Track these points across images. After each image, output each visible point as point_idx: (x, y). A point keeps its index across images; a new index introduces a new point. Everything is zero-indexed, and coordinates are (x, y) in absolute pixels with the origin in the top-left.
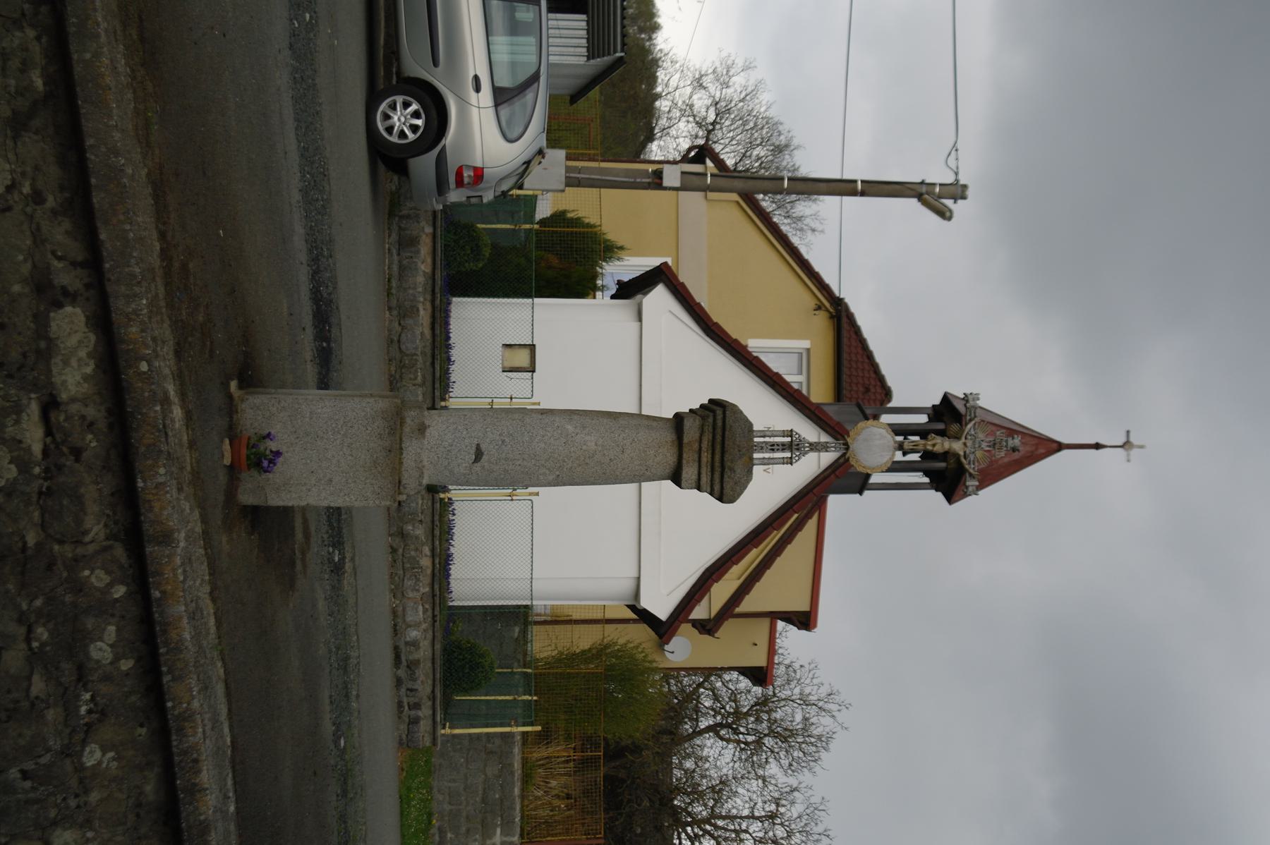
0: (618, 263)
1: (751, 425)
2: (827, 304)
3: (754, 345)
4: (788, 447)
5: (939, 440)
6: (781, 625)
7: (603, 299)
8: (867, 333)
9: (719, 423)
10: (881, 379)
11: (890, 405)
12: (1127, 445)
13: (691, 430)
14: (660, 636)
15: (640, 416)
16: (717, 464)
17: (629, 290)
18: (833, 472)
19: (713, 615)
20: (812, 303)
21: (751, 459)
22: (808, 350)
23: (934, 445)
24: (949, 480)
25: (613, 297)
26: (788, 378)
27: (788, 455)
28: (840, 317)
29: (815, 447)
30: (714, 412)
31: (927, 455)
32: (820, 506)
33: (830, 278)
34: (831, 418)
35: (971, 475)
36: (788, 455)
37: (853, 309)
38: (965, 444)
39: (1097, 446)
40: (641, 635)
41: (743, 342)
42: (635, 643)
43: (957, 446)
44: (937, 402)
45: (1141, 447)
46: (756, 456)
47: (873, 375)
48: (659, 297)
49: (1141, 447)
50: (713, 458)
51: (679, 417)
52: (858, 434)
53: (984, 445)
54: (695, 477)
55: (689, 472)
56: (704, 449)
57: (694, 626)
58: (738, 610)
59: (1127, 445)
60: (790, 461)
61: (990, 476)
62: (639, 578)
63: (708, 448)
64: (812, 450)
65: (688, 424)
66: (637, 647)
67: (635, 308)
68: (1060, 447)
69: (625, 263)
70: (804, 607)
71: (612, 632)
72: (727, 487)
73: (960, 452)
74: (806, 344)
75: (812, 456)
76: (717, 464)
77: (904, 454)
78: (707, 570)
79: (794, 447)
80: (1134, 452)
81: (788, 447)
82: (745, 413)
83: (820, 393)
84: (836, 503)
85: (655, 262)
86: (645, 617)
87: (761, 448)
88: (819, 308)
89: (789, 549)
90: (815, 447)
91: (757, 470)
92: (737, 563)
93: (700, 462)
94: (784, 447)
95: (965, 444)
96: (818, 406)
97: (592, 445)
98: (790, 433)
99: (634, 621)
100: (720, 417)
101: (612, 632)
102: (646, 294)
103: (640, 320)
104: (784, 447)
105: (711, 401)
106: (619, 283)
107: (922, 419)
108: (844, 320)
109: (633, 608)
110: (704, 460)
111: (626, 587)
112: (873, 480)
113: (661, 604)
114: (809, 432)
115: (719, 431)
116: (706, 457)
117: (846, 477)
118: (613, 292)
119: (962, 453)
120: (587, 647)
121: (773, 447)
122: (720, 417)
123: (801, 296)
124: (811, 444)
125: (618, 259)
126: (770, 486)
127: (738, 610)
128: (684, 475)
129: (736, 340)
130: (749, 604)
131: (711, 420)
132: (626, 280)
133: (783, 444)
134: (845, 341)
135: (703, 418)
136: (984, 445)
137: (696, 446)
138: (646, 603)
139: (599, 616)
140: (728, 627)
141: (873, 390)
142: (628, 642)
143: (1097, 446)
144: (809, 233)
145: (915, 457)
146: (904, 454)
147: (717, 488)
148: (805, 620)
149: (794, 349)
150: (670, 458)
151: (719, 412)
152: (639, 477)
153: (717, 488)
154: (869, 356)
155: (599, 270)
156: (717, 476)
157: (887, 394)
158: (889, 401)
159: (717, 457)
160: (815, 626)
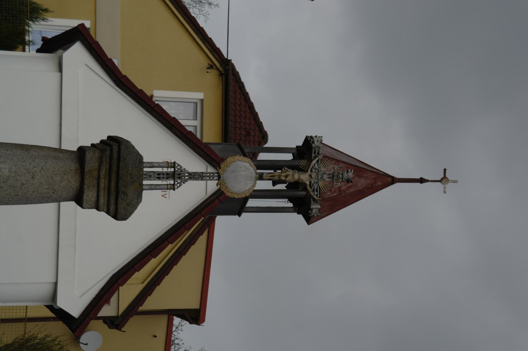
0: (42, 23)
1: (141, 158)
2: (218, 65)
3: (159, 95)
4: (172, 176)
5: (290, 172)
6: (177, 320)
7: (31, 52)
8: (249, 88)
9: (115, 155)
10: (259, 125)
11: (266, 146)
12: (444, 180)
13: (92, 161)
14: (73, 331)
15: (60, 150)
16: (113, 188)
17: (53, 45)
18: (218, 198)
19: (120, 312)
20: (205, 63)
21: (141, 185)
22: (202, 100)
23: (286, 176)
24: (305, 204)
25: (38, 51)
26: (183, 123)
27: (172, 182)
28: (227, 74)
29: (194, 176)
30: (110, 146)
31: (294, 185)
32: (209, 226)
33: (220, 43)
34: (216, 155)
35: (314, 200)
36: (172, 182)
37: (238, 69)
38: (310, 176)
39: (422, 181)
40: (58, 329)
41: (148, 94)
42: (53, 337)
43: (304, 177)
44: (300, 144)
45: (455, 182)
46: (145, 182)
47: (253, 122)
48: (77, 53)
49: (455, 182)
50: (109, 184)
51: (82, 149)
52: (227, 166)
53: (325, 177)
54: (94, 199)
55: (89, 195)
56: (102, 176)
57: (105, 322)
58: (141, 308)
59: (444, 180)
60: (173, 187)
61: (335, 203)
62: (56, 284)
63: (107, 176)
64: (190, 178)
65: (89, 156)
66: (54, 340)
67: (57, 61)
68: (393, 180)
69: (49, 23)
70: (194, 305)
71: (32, 328)
72: (121, 210)
73: (321, 183)
74: (200, 95)
75: (191, 184)
76: (113, 188)
77: (274, 184)
78: (114, 276)
79: (176, 176)
80: (449, 186)
81: (172, 176)
82: (137, 148)
83: (210, 135)
84: (223, 223)
85: (74, 23)
86: (61, 315)
87: (150, 176)
88: (211, 67)
89: (184, 259)
90: (194, 176)
91: (146, 194)
92: (138, 270)
93: (98, 186)
94: (168, 176)
95: (310, 176)
96: (207, 144)
97: (6, 172)
98: (169, 165)
99: (54, 319)
100: (115, 151)
101: (32, 328)
102: (65, 49)
103: (60, 70)
104: (168, 176)
105: (109, 137)
106: (44, 39)
107: (289, 157)
108: (231, 77)
109: (51, 308)
110: (102, 185)
111: (46, 290)
112: (251, 203)
113: (74, 304)
114: (192, 162)
115: (115, 162)
116: (103, 183)
117: (223, 203)
118: (39, 46)
119: (308, 183)
120: (10, 342)
121: (159, 176)
122: (115, 151)
123: (198, 58)
124: (190, 174)
125: (43, 20)
126: (158, 211)
127: (141, 308)
128: (85, 197)
129: (141, 90)
130: (151, 303)
131: (108, 153)
132: (49, 36)
133: (167, 174)
134: (231, 94)
135: (102, 151)
136: (325, 177)
137: (95, 173)
138: (61, 303)
139: (22, 315)
140: (133, 323)
141: (252, 134)
142: (47, 336)
143: (422, 181)
144: (207, 6)
145: (282, 187)
146: (274, 184)
147: (112, 208)
148: (196, 316)
149: (189, 100)
150: (73, 183)
151: (115, 147)
152: (58, 200)
153: (112, 208)
154: (250, 106)
155: (27, 28)
156: (113, 198)
157: (264, 137)
158: (266, 142)
159: (113, 183)
160: (204, 321)
